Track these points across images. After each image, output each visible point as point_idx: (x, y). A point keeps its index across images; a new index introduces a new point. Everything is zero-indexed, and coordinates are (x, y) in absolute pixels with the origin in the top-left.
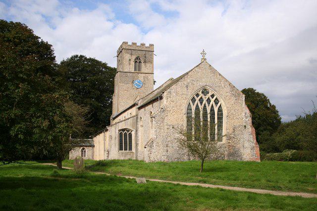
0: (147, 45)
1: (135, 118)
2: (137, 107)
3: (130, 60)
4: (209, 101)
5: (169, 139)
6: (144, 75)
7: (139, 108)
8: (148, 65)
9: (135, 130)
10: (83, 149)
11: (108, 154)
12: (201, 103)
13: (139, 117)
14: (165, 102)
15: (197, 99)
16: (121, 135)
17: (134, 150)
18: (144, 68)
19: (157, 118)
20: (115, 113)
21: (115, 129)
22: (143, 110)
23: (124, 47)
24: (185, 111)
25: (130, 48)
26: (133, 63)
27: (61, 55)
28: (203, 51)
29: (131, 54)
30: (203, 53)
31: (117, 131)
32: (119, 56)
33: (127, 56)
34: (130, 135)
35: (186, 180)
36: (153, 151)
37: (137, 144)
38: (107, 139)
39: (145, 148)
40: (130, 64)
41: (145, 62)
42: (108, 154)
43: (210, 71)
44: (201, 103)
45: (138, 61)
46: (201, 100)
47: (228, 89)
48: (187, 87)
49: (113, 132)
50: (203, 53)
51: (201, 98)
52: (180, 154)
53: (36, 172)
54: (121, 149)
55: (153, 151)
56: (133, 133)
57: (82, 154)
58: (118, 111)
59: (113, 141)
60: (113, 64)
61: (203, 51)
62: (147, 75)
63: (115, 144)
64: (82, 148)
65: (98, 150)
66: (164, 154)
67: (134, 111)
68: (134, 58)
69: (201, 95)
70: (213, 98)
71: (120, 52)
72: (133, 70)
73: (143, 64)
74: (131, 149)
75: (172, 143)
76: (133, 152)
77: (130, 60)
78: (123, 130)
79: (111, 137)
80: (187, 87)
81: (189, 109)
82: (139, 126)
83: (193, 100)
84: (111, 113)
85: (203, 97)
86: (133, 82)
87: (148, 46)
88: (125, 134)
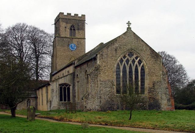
0: (80, 15)
4: (134, 61)
5: (102, 93)
6: (77, 40)
7: (76, 67)
8: (81, 31)
9: (72, 85)
12: (128, 64)
13: (76, 75)
15: (125, 60)
16: (61, 89)
17: (71, 101)
22: (78, 68)
24: (115, 69)
25: (66, 17)
28: (129, 22)
29: (67, 23)
30: (129, 23)
31: (58, 86)
34: (69, 89)
38: (50, 92)
39: (83, 99)
44: (128, 64)
45: (73, 29)
46: (128, 61)
47: (149, 52)
48: (116, 50)
50: (129, 23)
51: (128, 59)
54: (61, 100)
56: (71, 87)
59: (54, 94)
61: (129, 22)
62: (80, 40)
67: (71, 69)
68: (69, 26)
69: (127, 57)
70: (136, 59)
73: (77, 31)
79: (53, 90)
81: (118, 67)
82: (76, 82)
83: (121, 61)
85: (129, 58)
86: (68, 45)
87: (73, 15)
88: (65, 88)
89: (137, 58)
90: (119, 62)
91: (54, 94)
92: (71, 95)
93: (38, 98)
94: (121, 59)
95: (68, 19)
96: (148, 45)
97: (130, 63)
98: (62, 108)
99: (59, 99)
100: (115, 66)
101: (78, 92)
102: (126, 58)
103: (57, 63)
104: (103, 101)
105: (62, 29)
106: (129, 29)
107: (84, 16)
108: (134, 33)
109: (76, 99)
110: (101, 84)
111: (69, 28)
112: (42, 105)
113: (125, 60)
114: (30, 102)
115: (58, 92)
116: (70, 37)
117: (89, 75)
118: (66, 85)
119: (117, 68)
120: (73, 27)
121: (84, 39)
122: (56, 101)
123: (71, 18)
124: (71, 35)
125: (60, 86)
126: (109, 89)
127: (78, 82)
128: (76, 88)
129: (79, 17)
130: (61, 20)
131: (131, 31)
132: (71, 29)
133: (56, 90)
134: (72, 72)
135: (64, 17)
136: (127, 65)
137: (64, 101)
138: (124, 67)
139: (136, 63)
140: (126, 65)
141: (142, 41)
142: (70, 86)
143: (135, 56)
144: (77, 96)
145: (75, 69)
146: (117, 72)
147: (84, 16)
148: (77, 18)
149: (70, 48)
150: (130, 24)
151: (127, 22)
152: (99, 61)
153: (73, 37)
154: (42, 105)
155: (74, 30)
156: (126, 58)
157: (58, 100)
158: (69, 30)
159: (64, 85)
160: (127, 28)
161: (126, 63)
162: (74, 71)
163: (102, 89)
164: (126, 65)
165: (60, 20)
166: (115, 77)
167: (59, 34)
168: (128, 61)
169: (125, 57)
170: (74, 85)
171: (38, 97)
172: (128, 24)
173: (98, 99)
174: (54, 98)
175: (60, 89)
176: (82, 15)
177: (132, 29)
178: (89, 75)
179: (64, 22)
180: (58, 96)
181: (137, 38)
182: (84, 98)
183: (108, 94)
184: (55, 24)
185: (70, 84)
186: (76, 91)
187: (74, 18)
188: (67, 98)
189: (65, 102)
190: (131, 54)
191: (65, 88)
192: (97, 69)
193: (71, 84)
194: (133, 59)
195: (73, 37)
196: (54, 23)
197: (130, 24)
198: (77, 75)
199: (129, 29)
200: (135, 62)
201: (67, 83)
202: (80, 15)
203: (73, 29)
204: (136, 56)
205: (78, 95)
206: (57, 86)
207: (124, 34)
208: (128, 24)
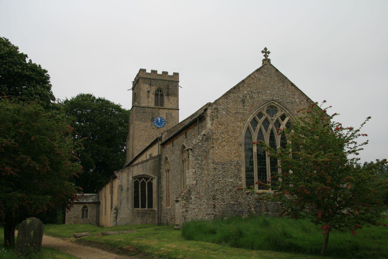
0: (171, 73)
1: (157, 159)
2: (160, 143)
3: (148, 92)
4: (278, 124)
5: (217, 187)
6: (166, 111)
7: (163, 145)
8: (172, 98)
9: (156, 177)
10: (85, 207)
11: (117, 213)
12: (266, 128)
13: (163, 157)
14: (209, 125)
15: (261, 121)
16: (136, 184)
17: (155, 208)
18: (167, 103)
19: (197, 151)
20: (129, 160)
21: (128, 176)
22: (169, 146)
23: (141, 75)
24: (242, 139)
25: (149, 76)
26: (152, 96)
27: (63, 90)
28: (266, 49)
29: (151, 85)
30: (266, 52)
31: (131, 179)
32: (135, 89)
33: (145, 87)
34: (150, 184)
35: (113, 230)
36: (191, 206)
37: (160, 198)
38: (116, 191)
39: (177, 201)
40: (148, 97)
41: (168, 95)
42: (117, 213)
43: (276, 79)
44: (266, 128)
45: (159, 94)
46: (266, 123)
48: (243, 101)
49: (124, 180)
50: (266, 52)
51: (266, 119)
52: (235, 211)
53: (108, 237)
54: (136, 205)
55: (191, 206)
56: (155, 182)
57: (83, 214)
58: (133, 156)
59: (124, 194)
60: (126, 104)
61: (266, 49)
62: (171, 111)
63: (128, 198)
64: (83, 206)
65: (104, 209)
66: (209, 211)
67: (155, 151)
68: (154, 89)
69: (266, 115)
70: (283, 120)
71: (136, 83)
72: (152, 105)
73: (166, 98)
74: (150, 205)
75: (222, 193)
76: (154, 211)
77: (148, 92)
78: (140, 177)
79: (121, 188)
80: (243, 101)
81: (248, 135)
82: (163, 171)
83: (254, 122)
84: (125, 161)
85: (270, 118)
86: (152, 120)
87: (172, 74)
88: (143, 184)
89: (283, 117)
90: (250, 125)
91: (124, 194)
92: (155, 196)
93: (101, 203)
94: (254, 119)
95: (153, 79)
96: (303, 94)
97: (270, 127)
98: (138, 221)
99: (132, 205)
100: (244, 132)
101: (168, 189)
102: (263, 118)
103: (134, 148)
104: (220, 205)
105: (143, 94)
106: (266, 61)
107: (176, 75)
108: (277, 70)
109: (164, 204)
110: (215, 168)
111: (155, 93)
112: (105, 215)
113: (262, 122)
114: (87, 210)
115: (130, 191)
116: (155, 107)
117: (190, 151)
118: (145, 178)
119: (246, 137)
120: (161, 91)
121: (177, 109)
122: (127, 209)
123: (157, 77)
124: (156, 104)
125: (134, 179)
126: (232, 180)
127: (168, 171)
128: (164, 183)
129: (170, 76)
130: (143, 80)
131: (271, 65)
132: (156, 95)
133: (126, 188)
134: (158, 154)
135: (145, 76)
136: (266, 131)
137: (148, 207)
138: (261, 136)
139: (283, 127)
140: (263, 130)
141: (292, 85)
142: (152, 179)
143: (279, 114)
144: (165, 198)
145: (161, 149)
146: (246, 144)
147: (176, 75)
148: (166, 78)
149: (156, 124)
150: (269, 53)
151: (263, 49)
152: (211, 122)
153: (159, 107)
154: (105, 215)
155: (162, 95)
156: (263, 118)
157: (130, 206)
158: (153, 96)
159: (142, 178)
160: (264, 60)
161: (263, 127)
162: (161, 151)
163: (217, 179)
164: (263, 130)
165: (140, 81)
166: (243, 154)
167: (139, 103)
168: (266, 123)
169: (260, 115)
170: (159, 178)
171: (101, 201)
172: (264, 54)
173: (208, 199)
174: (124, 202)
175: (134, 185)
176: (174, 73)
177: (272, 63)
178: (190, 151)
179: (146, 83)
180: (130, 199)
181: (283, 79)
182: (180, 199)
183: (230, 191)
184: (133, 89)
185: (153, 176)
186: (164, 189)
187: (161, 78)
188: (147, 201)
189: (150, 209)
190: (272, 110)
191: (143, 184)
192: (208, 139)
193: (155, 175)
194: (276, 119)
195: (160, 107)
196: (131, 86)
197: (269, 53)
198: (166, 159)
199: (266, 61)
200: (280, 125)
201: (148, 174)
202: (171, 73)
203: (159, 94)
204: (283, 113)
205: (168, 196)
206: (128, 180)
207: (258, 70)
208: (264, 54)
